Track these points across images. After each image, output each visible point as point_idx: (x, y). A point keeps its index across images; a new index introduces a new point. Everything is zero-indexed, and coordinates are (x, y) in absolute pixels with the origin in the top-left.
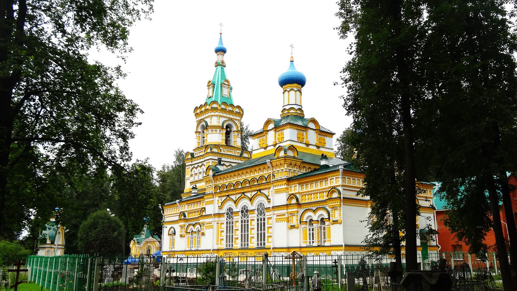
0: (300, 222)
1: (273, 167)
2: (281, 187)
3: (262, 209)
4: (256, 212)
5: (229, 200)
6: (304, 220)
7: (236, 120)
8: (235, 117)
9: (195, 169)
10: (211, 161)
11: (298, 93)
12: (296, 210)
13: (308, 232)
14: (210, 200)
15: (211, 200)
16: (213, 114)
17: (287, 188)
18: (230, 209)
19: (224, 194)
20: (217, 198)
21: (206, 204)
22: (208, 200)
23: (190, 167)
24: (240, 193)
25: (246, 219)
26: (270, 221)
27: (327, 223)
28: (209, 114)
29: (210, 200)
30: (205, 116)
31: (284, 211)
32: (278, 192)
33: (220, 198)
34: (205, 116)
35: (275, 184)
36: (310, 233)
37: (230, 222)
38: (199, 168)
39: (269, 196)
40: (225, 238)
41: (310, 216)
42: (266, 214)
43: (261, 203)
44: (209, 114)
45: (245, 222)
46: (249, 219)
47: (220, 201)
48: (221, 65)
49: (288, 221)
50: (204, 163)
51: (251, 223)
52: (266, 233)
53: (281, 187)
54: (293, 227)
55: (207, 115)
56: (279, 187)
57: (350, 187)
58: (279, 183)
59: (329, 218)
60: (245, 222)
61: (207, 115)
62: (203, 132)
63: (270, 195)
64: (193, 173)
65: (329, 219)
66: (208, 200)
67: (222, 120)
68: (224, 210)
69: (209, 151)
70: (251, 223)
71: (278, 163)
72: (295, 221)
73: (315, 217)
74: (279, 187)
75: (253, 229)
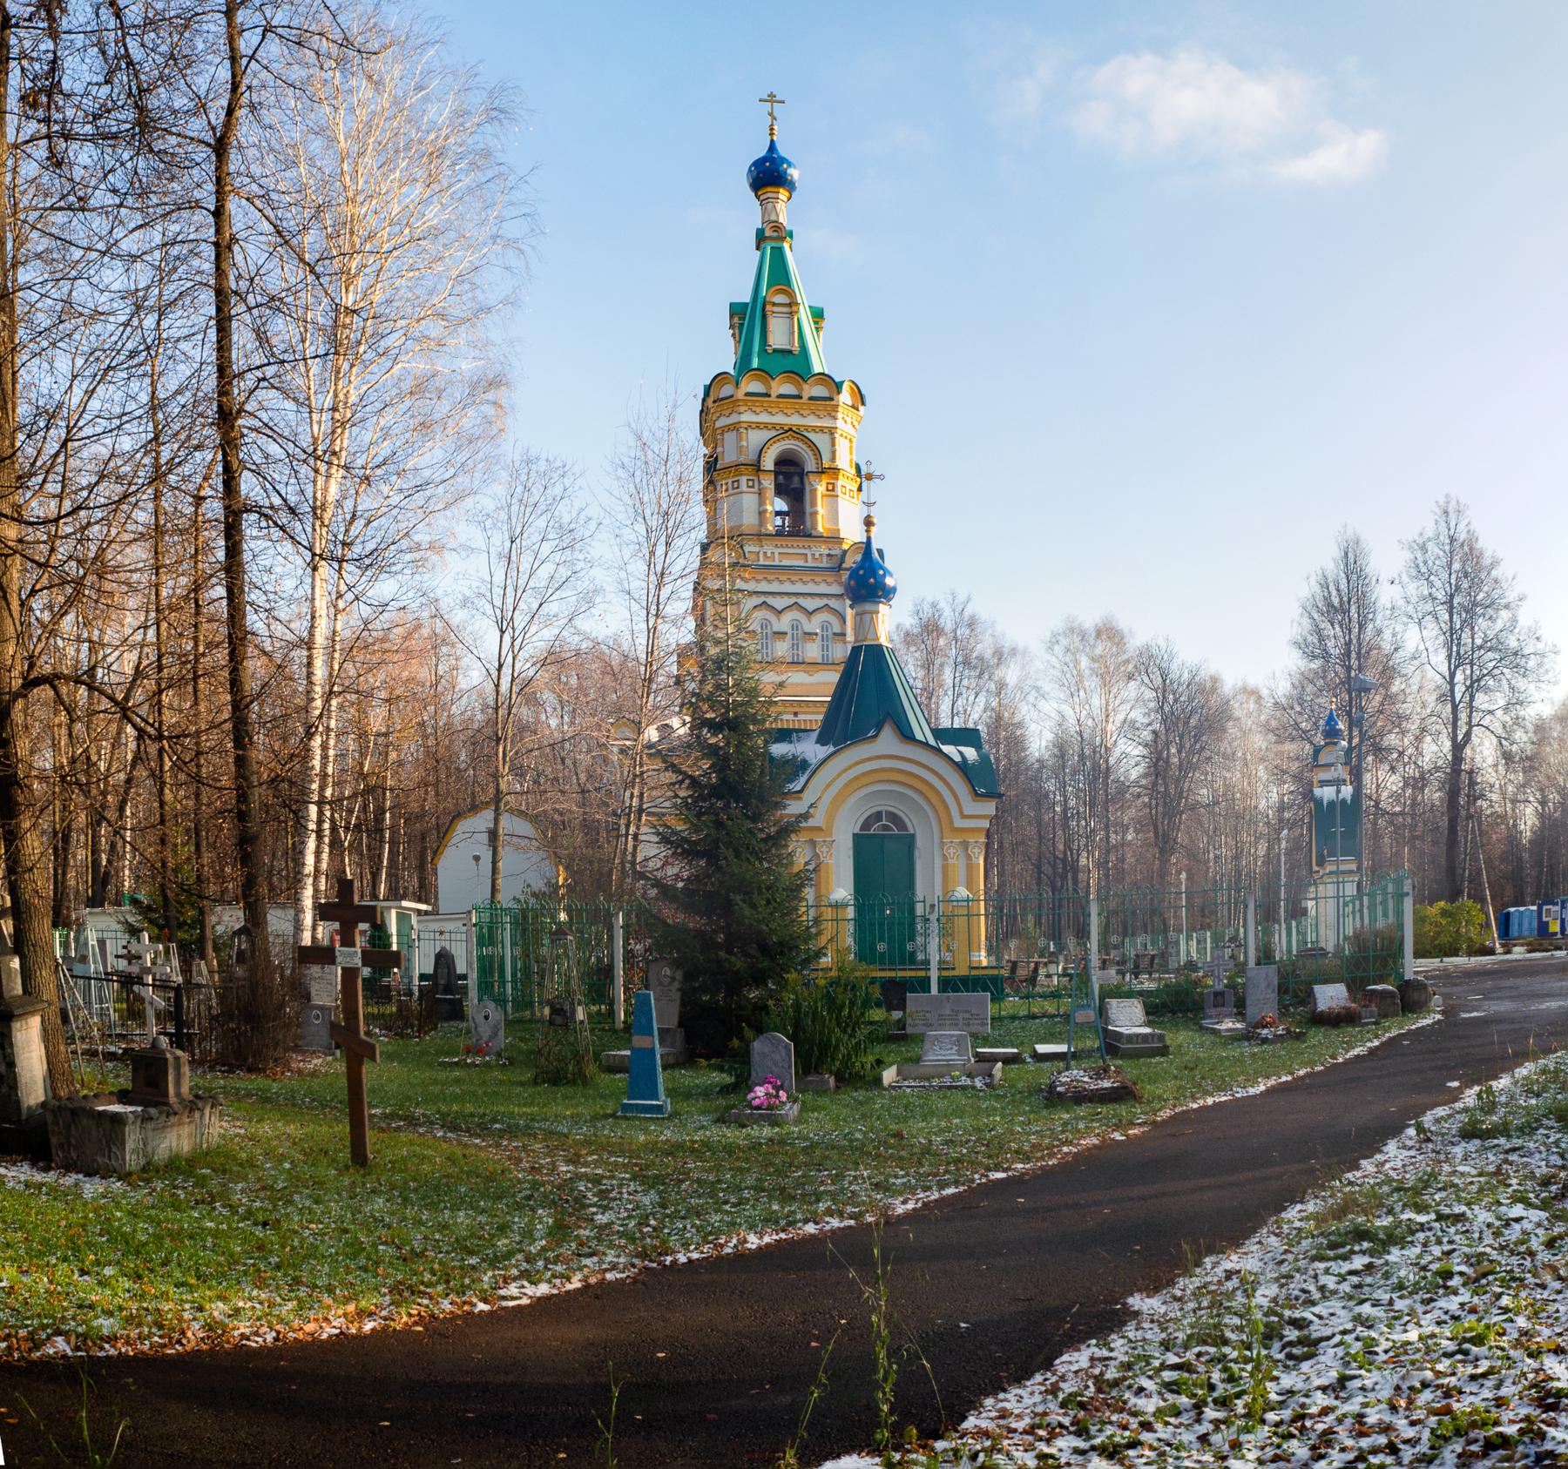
7: (814, 429)
8: (812, 421)
48: (771, 238)
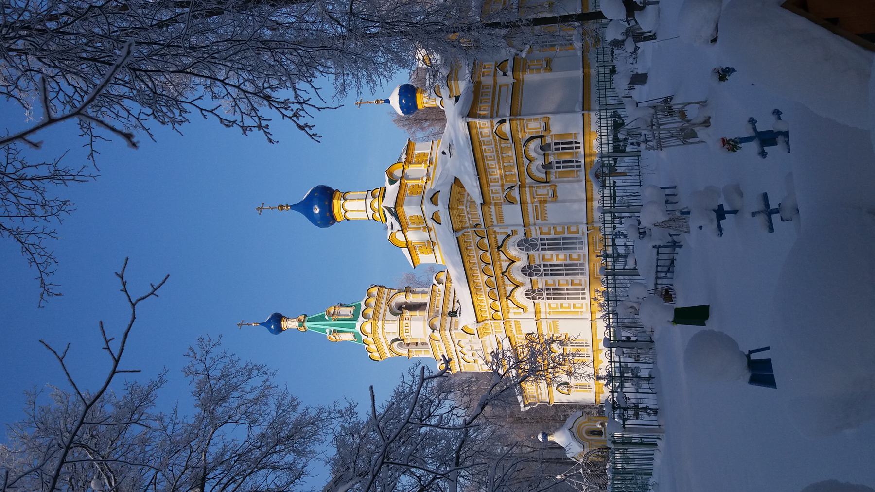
0: (547, 182)
1: (463, 228)
2: (493, 213)
3: (526, 244)
4: (531, 253)
5: (509, 273)
6: (544, 176)
9: (466, 357)
10: (452, 332)
11: (347, 196)
12: (527, 189)
13: (562, 169)
14: (513, 327)
15: (513, 324)
16: (380, 331)
17: (496, 204)
18: (523, 271)
19: (500, 281)
20: (511, 316)
21: (520, 333)
22: (514, 329)
23: (462, 365)
24: (502, 278)
25: (542, 269)
26: (545, 230)
27: (548, 140)
28: (381, 336)
29: (513, 327)
30: (384, 344)
31: (530, 208)
32: (500, 218)
33: (511, 311)
34: (384, 344)
35: (489, 224)
36: (564, 167)
37: (542, 245)
38: (464, 350)
39: (506, 233)
40: (569, 278)
41: (537, 169)
42: (534, 236)
43: (526, 294)
44: (381, 336)
45: (547, 270)
46: (542, 263)
47: (515, 311)
49: (545, 201)
50: (456, 342)
51: (551, 285)
52: (564, 236)
53: (493, 213)
54: (554, 195)
55: (382, 340)
56: (494, 217)
57: (493, 98)
58: (488, 217)
59: (541, 137)
60: (547, 270)
61: (382, 340)
62: (408, 345)
63: (506, 230)
64: (472, 360)
65: (543, 136)
66: (514, 329)
67: (389, 316)
68: (529, 304)
69: (437, 334)
70: (551, 285)
71: (457, 220)
72: (544, 191)
73: (540, 161)
74: (494, 217)
75: (562, 305)
